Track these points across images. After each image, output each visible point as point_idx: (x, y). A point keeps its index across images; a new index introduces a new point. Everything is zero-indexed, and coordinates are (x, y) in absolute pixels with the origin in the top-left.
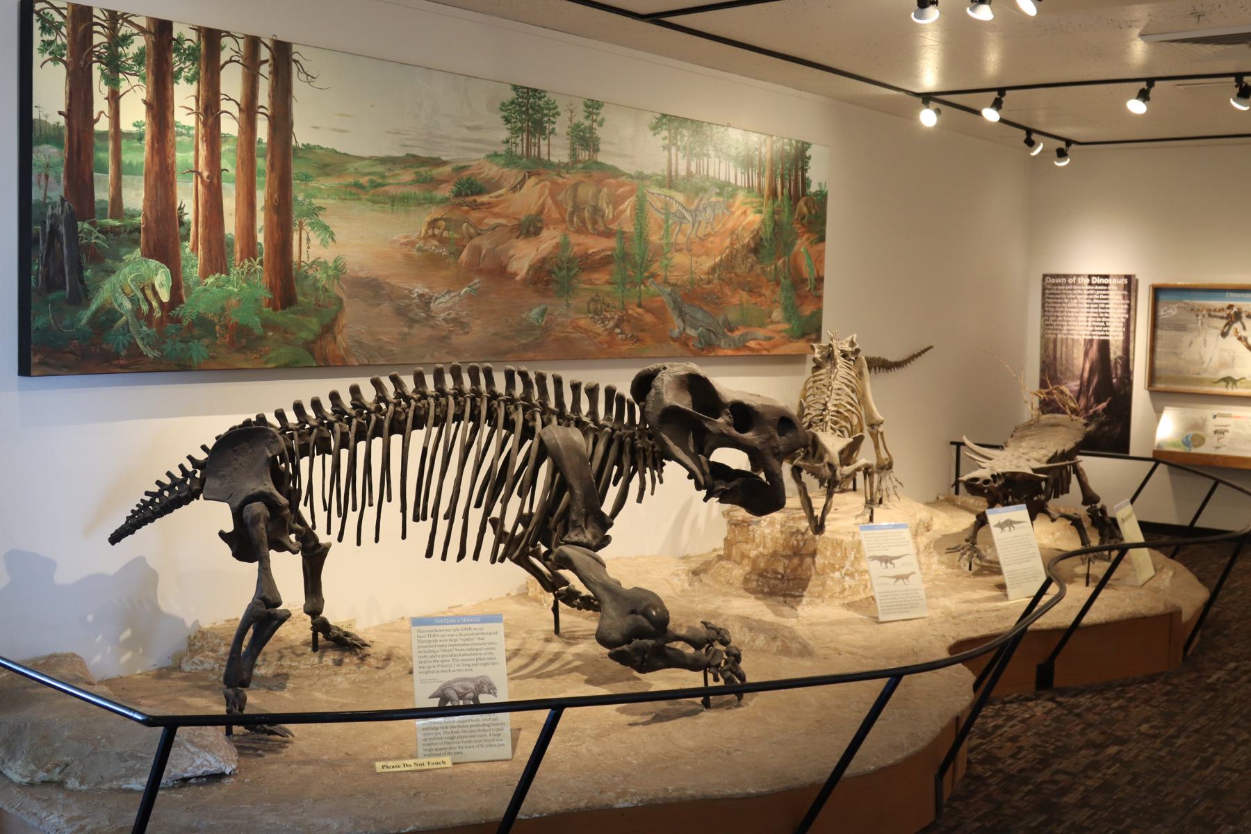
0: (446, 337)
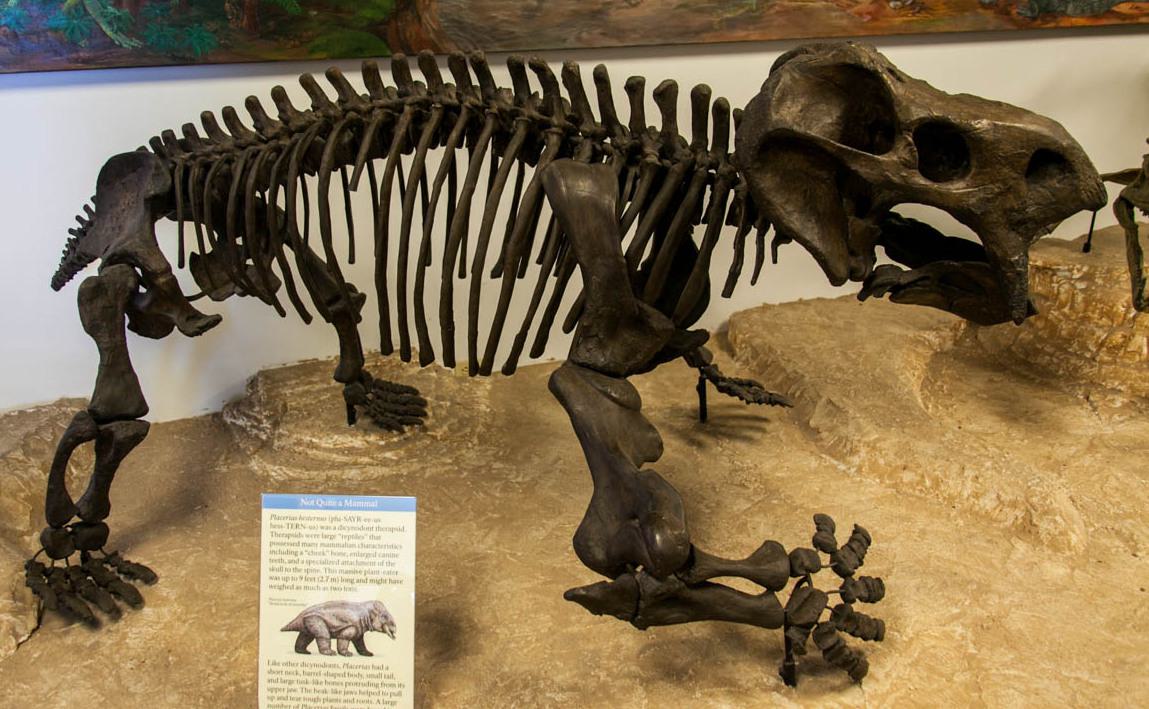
0: (599, 12)
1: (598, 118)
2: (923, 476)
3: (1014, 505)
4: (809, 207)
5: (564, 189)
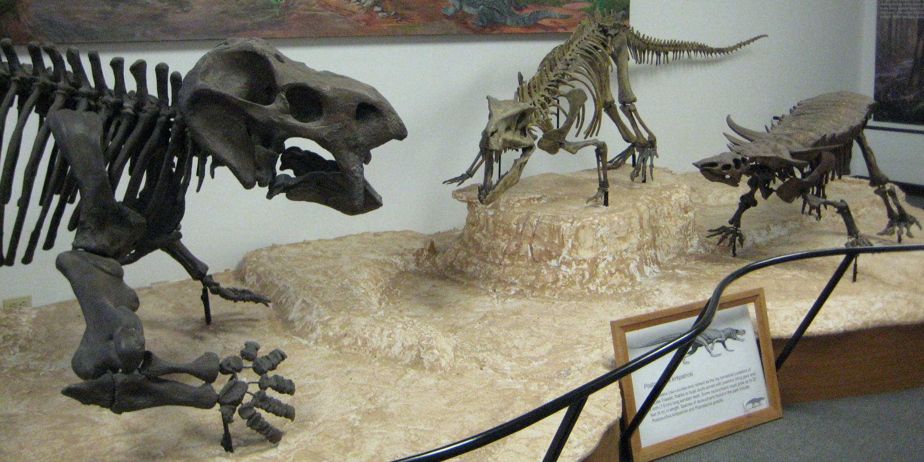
1: (93, 84)
2: (356, 339)
3: (411, 348)
4: (228, 139)
5: (64, 129)
